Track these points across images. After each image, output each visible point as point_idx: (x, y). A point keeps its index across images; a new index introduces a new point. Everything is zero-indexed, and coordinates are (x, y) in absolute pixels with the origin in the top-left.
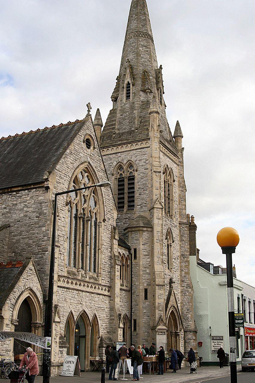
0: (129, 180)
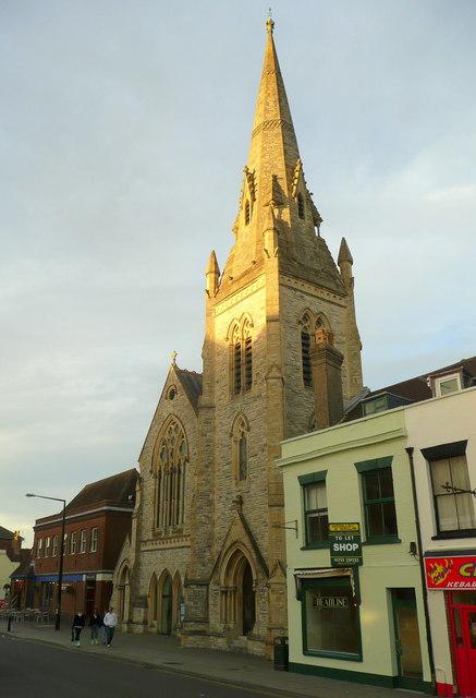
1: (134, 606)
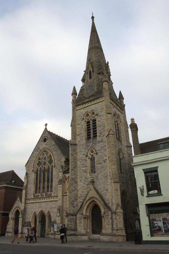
0: (93, 121)
1: (24, 226)
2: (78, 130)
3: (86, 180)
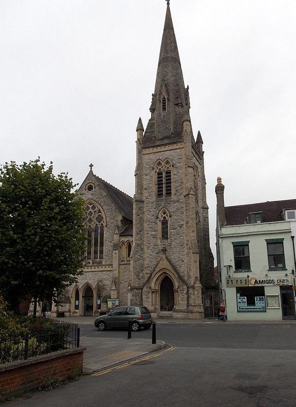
2: (145, 182)
3: (156, 247)
